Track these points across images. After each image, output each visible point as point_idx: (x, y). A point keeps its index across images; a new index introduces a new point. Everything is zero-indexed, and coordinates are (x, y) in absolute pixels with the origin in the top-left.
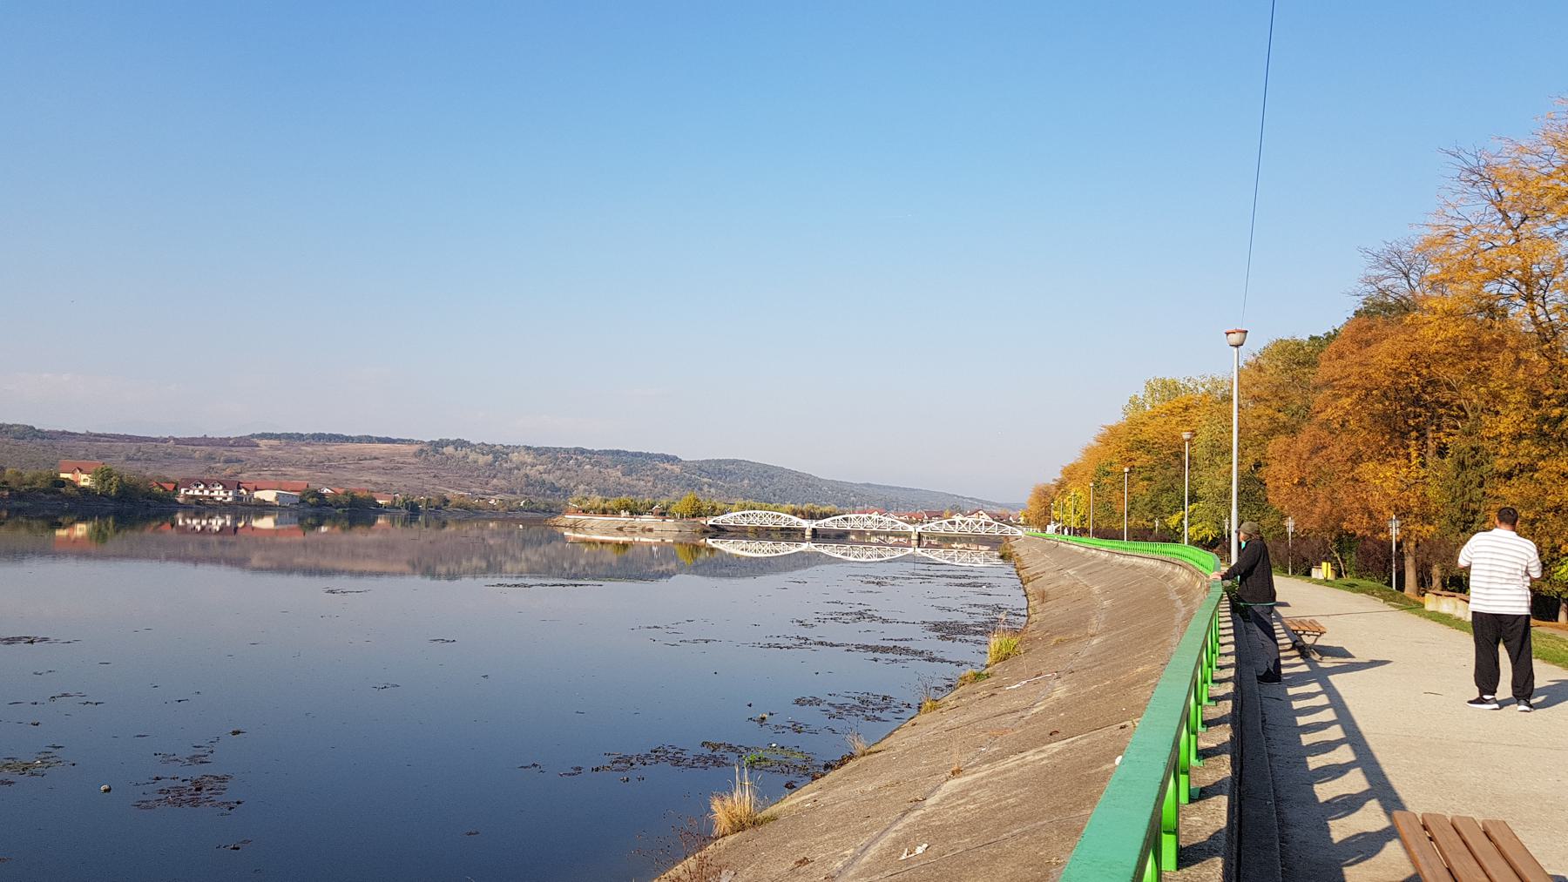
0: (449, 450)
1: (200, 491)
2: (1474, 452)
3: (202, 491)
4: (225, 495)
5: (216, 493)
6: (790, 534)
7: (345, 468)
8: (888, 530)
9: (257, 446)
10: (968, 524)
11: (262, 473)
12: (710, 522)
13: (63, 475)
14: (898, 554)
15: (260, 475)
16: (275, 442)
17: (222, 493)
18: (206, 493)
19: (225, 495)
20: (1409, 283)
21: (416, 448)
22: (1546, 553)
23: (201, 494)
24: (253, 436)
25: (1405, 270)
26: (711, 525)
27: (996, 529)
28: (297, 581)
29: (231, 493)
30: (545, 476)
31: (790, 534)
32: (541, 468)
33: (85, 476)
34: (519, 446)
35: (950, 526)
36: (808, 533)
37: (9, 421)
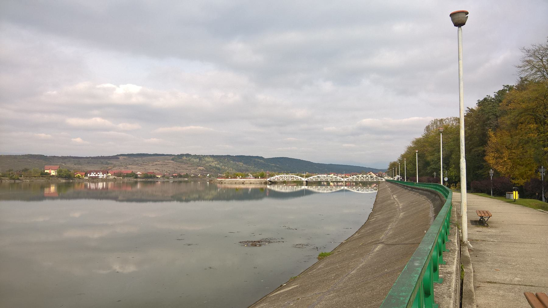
0: (184, 158)
1: (95, 175)
2: (510, 135)
3: (95, 175)
4: (103, 176)
5: (100, 175)
6: (300, 183)
7: (148, 165)
8: (334, 180)
9: (119, 158)
10: (364, 177)
11: (120, 168)
12: (268, 179)
13: (46, 171)
14: (338, 189)
15: (119, 168)
16: (125, 157)
17: (102, 175)
18: (97, 175)
19: (103, 176)
20: (543, 64)
21: (171, 158)
22: (381, 172)
23: (95, 176)
24: (118, 155)
25: (541, 58)
26: (269, 181)
27: (375, 179)
28: (134, 205)
29: (105, 175)
30: (217, 165)
31: (300, 183)
32: (216, 163)
33: (53, 171)
34: (208, 155)
35: (357, 178)
36: (305, 183)
37: (3, 154)
